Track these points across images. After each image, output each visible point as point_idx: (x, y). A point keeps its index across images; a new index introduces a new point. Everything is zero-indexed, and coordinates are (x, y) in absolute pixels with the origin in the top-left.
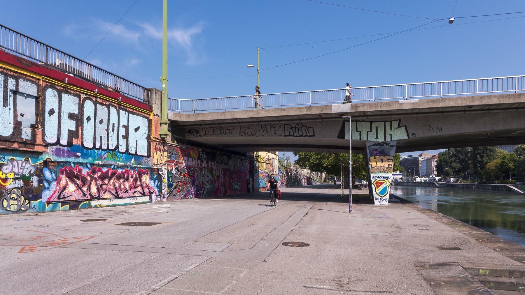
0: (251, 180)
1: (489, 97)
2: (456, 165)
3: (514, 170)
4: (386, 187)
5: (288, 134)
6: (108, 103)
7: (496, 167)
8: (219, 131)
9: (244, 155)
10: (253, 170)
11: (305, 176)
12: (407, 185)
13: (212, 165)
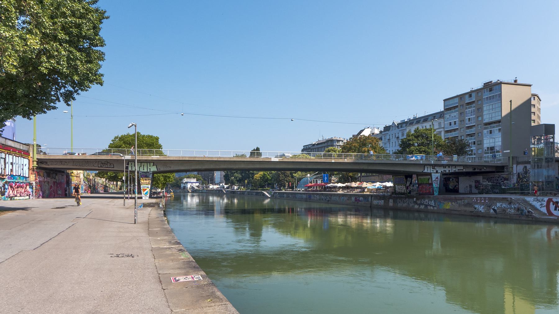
0: (68, 188)
1: (185, 157)
2: (237, 175)
3: (271, 180)
4: (147, 191)
5: (100, 166)
6: (18, 155)
7: (261, 177)
8: (60, 163)
9: (63, 172)
10: (69, 182)
11: (102, 185)
12: (202, 192)
13: (49, 179)
